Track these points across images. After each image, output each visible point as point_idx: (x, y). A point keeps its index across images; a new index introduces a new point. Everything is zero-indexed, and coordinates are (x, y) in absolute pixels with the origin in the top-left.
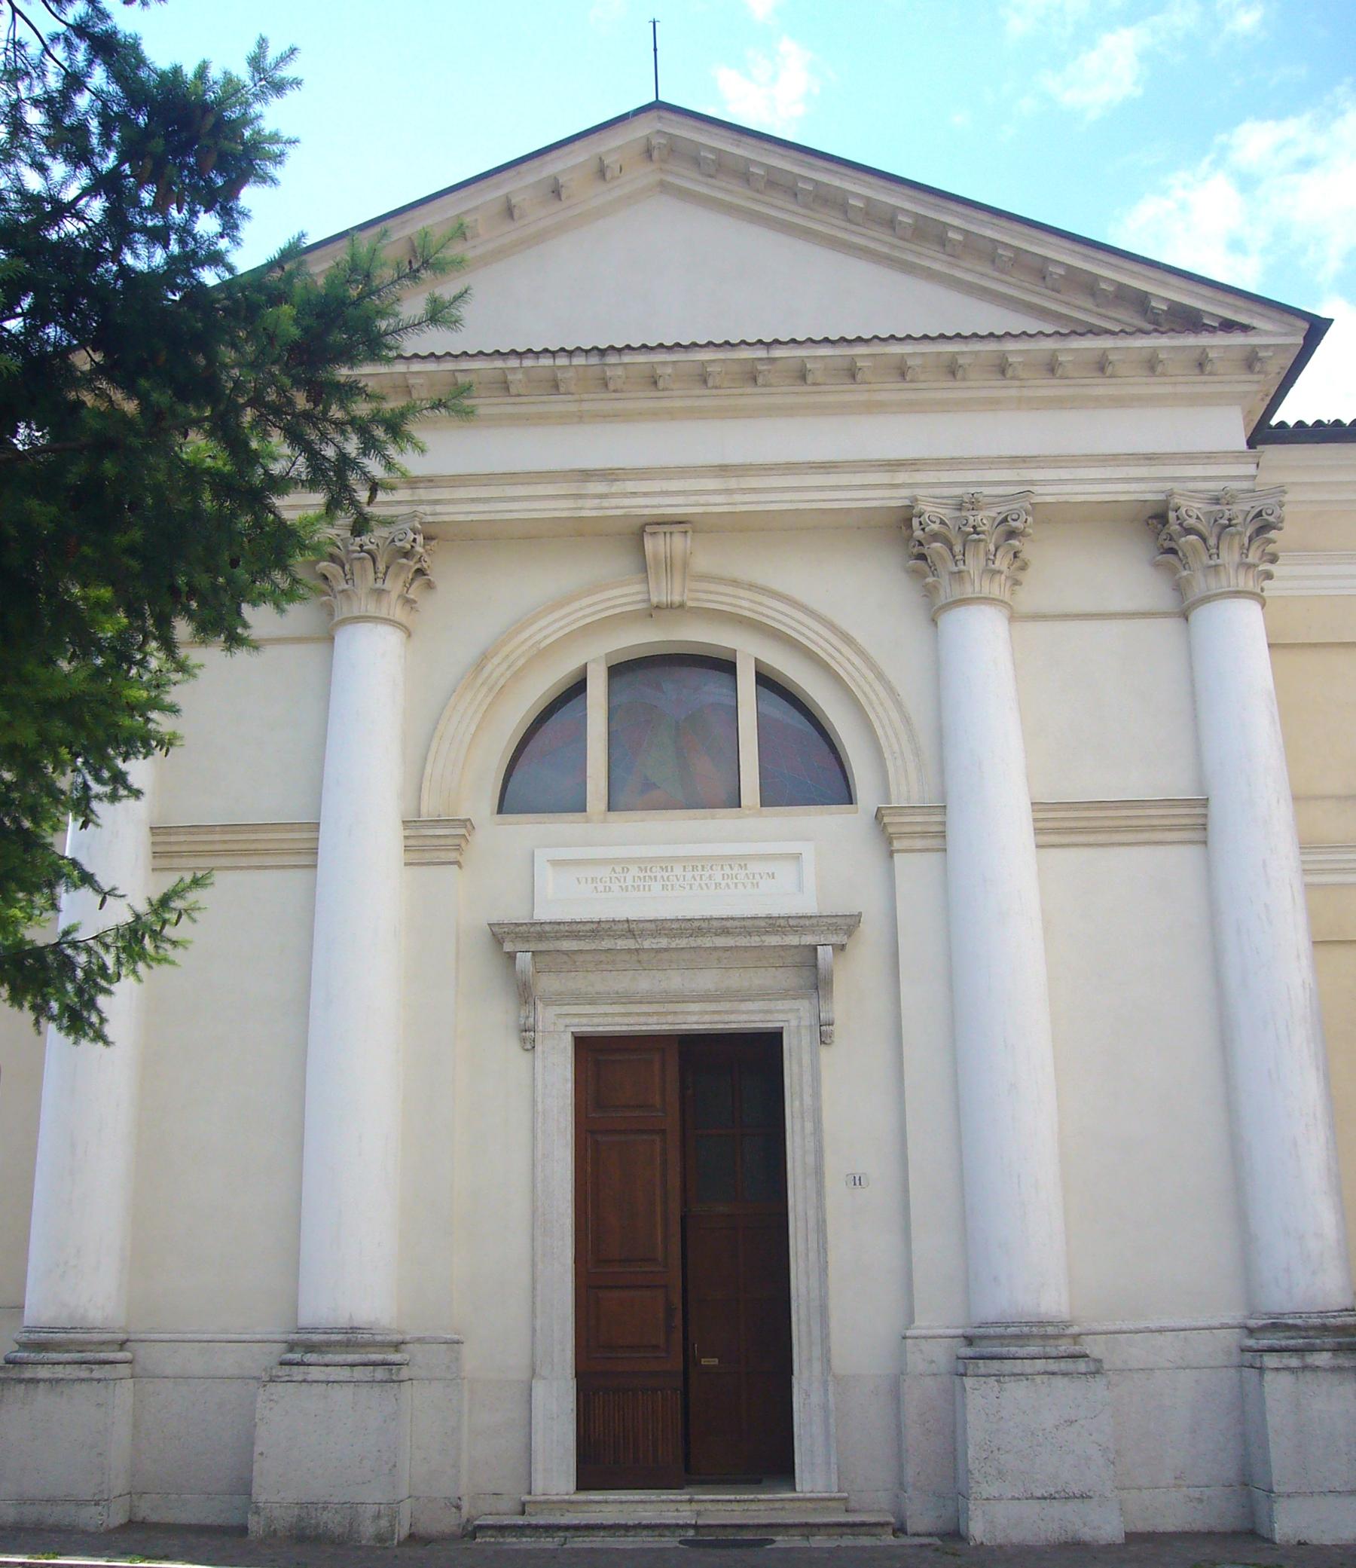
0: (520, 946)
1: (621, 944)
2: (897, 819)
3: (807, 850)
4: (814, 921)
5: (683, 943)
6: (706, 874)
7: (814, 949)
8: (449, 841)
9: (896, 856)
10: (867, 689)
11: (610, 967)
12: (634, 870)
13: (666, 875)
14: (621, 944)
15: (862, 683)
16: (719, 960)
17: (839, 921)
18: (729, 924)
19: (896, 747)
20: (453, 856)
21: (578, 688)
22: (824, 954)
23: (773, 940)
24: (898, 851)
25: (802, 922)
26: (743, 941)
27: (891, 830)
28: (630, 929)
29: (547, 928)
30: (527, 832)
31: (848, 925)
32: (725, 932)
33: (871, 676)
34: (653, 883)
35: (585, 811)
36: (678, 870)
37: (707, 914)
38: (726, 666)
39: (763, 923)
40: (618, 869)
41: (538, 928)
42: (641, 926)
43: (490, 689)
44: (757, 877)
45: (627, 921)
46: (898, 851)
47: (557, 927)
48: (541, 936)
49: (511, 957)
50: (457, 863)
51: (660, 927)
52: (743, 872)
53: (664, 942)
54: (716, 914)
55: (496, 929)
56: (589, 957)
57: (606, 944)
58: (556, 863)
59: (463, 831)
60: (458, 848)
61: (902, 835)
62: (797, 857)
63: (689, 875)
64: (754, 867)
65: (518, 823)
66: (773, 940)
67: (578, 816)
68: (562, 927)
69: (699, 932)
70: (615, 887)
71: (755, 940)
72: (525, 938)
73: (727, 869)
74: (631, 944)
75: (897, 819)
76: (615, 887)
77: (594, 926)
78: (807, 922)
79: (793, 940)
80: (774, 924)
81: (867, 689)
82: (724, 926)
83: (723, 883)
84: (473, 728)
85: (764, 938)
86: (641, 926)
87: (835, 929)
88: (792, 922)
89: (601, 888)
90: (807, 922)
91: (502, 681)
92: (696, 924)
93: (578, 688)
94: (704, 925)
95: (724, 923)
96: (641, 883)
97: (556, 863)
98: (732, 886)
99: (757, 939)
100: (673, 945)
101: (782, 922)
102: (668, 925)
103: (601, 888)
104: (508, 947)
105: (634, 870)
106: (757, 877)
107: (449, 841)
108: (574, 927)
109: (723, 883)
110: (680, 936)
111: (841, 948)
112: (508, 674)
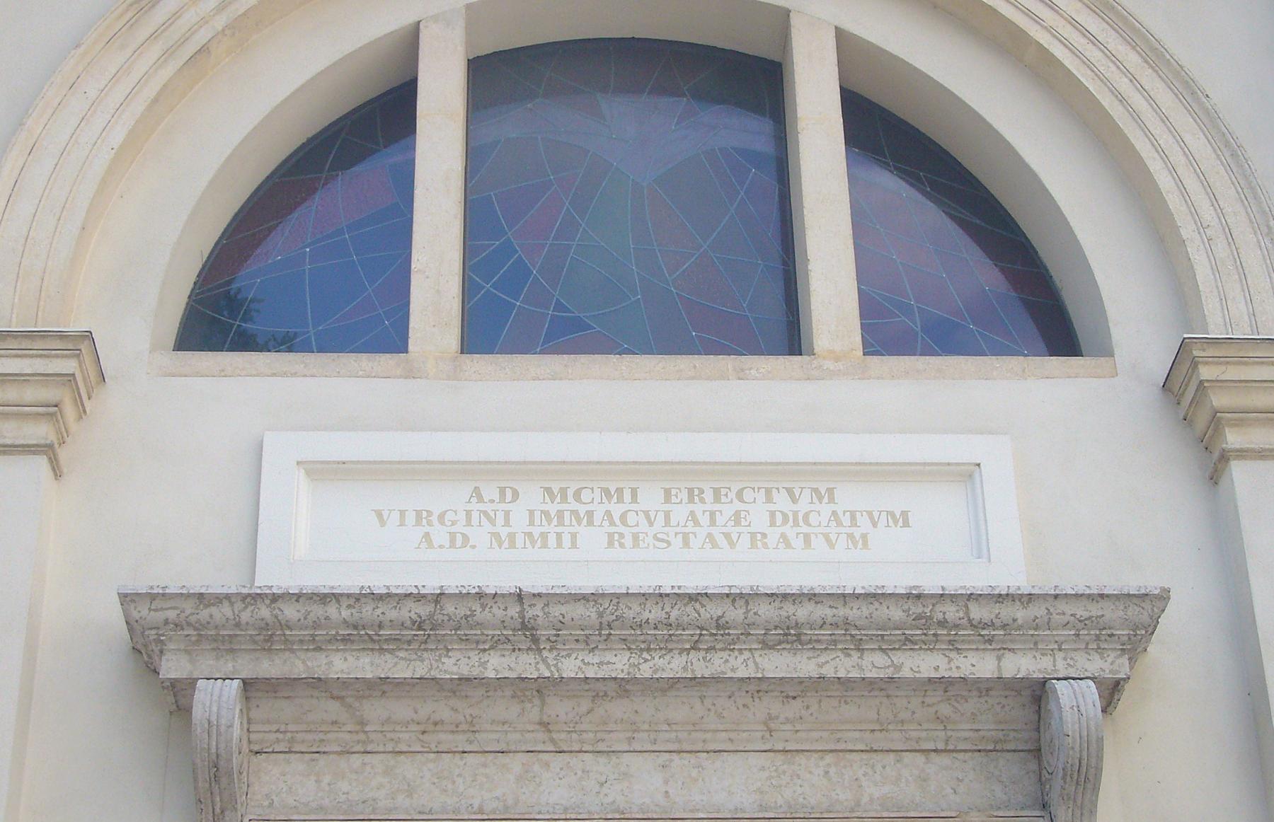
0: (207, 663)
1: (497, 665)
2: (1232, 373)
3: (996, 457)
4: (1038, 610)
5: (673, 665)
6: (727, 510)
7: (1037, 693)
8: (31, 394)
9: (1239, 471)
10: (1124, 85)
11: (460, 741)
12: (532, 496)
13: (616, 510)
14: (497, 665)
15: (1110, 71)
16: (769, 726)
17: (1110, 613)
18: (803, 612)
19: (1208, 214)
20: (39, 432)
21: (383, 116)
22: (1075, 700)
23: (925, 664)
24: (1243, 454)
25: (1007, 612)
26: (841, 665)
27: (1219, 400)
28: (527, 620)
29: (290, 612)
30: (245, 388)
31: (1127, 623)
32: (791, 636)
33: (1132, 59)
34: (582, 530)
35: (405, 349)
36: (651, 497)
37: (742, 581)
38: (756, 82)
39: (896, 614)
40: (490, 492)
41: (264, 612)
42: (556, 611)
43: (168, 54)
44: (863, 521)
45: (519, 597)
46: (1243, 454)
47: (317, 611)
48: (271, 637)
49: (179, 697)
50: (47, 450)
51: (612, 618)
52: (826, 509)
53: (618, 663)
54: (770, 581)
55: (142, 611)
56: (401, 709)
57: (455, 665)
58: (320, 471)
59: (69, 366)
60: (51, 412)
61: (1244, 417)
62: (967, 474)
63: (680, 512)
64: (850, 497)
65: (223, 374)
66: (925, 664)
67: (386, 361)
68: (332, 610)
69: (719, 635)
70: (480, 535)
71: (874, 664)
72: (222, 641)
73: (782, 502)
74: (526, 665)
75: (1232, 373)
76: (480, 535)
77: (424, 610)
78: (1021, 614)
79: (980, 665)
80: (928, 617)
81: (1124, 85)
82: (789, 620)
83: (774, 535)
84: (118, 136)
85: (898, 658)
86: (556, 611)
87: (1094, 634)
88: (978, 612)
89: (440, 535)
90: (1021, 614)
91: (202, 37)
92: (712, 610)
93: (383, 116)
94: (735, 614)
95: (789, 608)
96: (552, 529)
97: (320, 471)
98: (799, 542)
99: (880, 659)
100: (645, 671)
101: (951, 612)
102: (631, 611)
103: (440, 535)
104: (173, 667)
105: (532, 496)
106: (863, 521)
107: (31, 394)
108: (368, 612)
109: (774, 535)
110: (666, 646)
111: (1111, 691)
112: (220, 22)
